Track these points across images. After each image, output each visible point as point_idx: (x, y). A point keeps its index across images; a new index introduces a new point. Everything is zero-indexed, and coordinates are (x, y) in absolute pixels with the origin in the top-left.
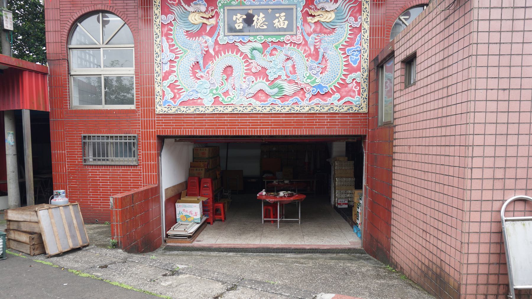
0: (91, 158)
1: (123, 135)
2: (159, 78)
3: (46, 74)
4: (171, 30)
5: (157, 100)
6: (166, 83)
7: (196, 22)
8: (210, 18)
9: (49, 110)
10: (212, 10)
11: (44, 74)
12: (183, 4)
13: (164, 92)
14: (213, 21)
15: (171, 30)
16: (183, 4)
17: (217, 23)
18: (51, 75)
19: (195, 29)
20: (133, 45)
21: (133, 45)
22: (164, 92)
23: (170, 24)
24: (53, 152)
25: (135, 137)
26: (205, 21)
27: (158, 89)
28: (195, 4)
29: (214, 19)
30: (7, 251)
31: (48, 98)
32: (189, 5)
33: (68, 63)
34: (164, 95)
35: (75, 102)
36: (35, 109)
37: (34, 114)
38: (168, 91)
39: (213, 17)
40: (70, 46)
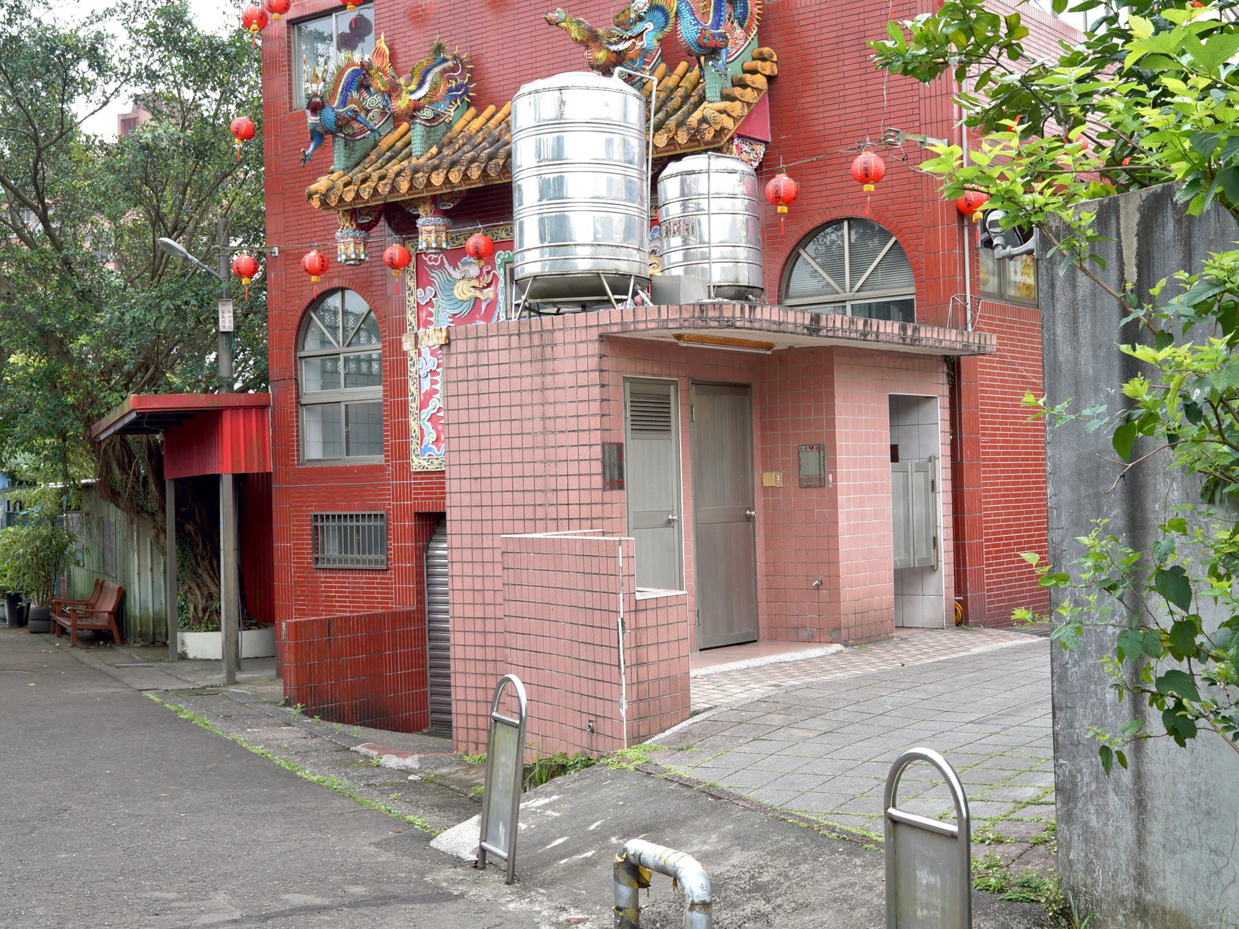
0: (332, 549)
1: (367, 513)
2: (414, 405)
3: (267, 406)
4: (431, 315)
5: (413, 447)
6: (426, 413)
7: (465, 297)
8: (484, 288)
9: (271, 468)
10: (488, 273)
11: (262, 408)
12: (447, 266)
13: (421, 430)
14: (489, 293)
15: (431, 315)
16: (447, 266)
17: (497, 295)
18: (274, 407)
19: (465, 309)
20: (913, 290)
21: (913, 290)
22: (421, 430)
23: (430, 303)
24: (275, 545)
25: (382, 516)
26: (478, 294)
27: (413, 425)
28: (464, 264)
29: (492, 288)
30: (846, 224)
31: (269, 447)
32: (455, 267)
33: (297, 384)
34: (422, 436)
35: (313, 448)
36: (243, 471)
37: (240, 480)
38: (428, 427)
39: (489, 285)
40: (302, 354)
